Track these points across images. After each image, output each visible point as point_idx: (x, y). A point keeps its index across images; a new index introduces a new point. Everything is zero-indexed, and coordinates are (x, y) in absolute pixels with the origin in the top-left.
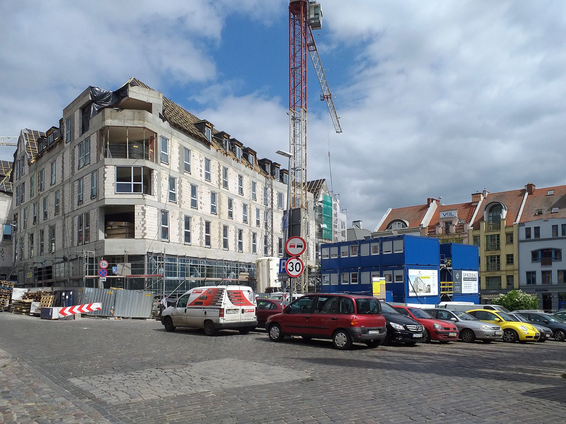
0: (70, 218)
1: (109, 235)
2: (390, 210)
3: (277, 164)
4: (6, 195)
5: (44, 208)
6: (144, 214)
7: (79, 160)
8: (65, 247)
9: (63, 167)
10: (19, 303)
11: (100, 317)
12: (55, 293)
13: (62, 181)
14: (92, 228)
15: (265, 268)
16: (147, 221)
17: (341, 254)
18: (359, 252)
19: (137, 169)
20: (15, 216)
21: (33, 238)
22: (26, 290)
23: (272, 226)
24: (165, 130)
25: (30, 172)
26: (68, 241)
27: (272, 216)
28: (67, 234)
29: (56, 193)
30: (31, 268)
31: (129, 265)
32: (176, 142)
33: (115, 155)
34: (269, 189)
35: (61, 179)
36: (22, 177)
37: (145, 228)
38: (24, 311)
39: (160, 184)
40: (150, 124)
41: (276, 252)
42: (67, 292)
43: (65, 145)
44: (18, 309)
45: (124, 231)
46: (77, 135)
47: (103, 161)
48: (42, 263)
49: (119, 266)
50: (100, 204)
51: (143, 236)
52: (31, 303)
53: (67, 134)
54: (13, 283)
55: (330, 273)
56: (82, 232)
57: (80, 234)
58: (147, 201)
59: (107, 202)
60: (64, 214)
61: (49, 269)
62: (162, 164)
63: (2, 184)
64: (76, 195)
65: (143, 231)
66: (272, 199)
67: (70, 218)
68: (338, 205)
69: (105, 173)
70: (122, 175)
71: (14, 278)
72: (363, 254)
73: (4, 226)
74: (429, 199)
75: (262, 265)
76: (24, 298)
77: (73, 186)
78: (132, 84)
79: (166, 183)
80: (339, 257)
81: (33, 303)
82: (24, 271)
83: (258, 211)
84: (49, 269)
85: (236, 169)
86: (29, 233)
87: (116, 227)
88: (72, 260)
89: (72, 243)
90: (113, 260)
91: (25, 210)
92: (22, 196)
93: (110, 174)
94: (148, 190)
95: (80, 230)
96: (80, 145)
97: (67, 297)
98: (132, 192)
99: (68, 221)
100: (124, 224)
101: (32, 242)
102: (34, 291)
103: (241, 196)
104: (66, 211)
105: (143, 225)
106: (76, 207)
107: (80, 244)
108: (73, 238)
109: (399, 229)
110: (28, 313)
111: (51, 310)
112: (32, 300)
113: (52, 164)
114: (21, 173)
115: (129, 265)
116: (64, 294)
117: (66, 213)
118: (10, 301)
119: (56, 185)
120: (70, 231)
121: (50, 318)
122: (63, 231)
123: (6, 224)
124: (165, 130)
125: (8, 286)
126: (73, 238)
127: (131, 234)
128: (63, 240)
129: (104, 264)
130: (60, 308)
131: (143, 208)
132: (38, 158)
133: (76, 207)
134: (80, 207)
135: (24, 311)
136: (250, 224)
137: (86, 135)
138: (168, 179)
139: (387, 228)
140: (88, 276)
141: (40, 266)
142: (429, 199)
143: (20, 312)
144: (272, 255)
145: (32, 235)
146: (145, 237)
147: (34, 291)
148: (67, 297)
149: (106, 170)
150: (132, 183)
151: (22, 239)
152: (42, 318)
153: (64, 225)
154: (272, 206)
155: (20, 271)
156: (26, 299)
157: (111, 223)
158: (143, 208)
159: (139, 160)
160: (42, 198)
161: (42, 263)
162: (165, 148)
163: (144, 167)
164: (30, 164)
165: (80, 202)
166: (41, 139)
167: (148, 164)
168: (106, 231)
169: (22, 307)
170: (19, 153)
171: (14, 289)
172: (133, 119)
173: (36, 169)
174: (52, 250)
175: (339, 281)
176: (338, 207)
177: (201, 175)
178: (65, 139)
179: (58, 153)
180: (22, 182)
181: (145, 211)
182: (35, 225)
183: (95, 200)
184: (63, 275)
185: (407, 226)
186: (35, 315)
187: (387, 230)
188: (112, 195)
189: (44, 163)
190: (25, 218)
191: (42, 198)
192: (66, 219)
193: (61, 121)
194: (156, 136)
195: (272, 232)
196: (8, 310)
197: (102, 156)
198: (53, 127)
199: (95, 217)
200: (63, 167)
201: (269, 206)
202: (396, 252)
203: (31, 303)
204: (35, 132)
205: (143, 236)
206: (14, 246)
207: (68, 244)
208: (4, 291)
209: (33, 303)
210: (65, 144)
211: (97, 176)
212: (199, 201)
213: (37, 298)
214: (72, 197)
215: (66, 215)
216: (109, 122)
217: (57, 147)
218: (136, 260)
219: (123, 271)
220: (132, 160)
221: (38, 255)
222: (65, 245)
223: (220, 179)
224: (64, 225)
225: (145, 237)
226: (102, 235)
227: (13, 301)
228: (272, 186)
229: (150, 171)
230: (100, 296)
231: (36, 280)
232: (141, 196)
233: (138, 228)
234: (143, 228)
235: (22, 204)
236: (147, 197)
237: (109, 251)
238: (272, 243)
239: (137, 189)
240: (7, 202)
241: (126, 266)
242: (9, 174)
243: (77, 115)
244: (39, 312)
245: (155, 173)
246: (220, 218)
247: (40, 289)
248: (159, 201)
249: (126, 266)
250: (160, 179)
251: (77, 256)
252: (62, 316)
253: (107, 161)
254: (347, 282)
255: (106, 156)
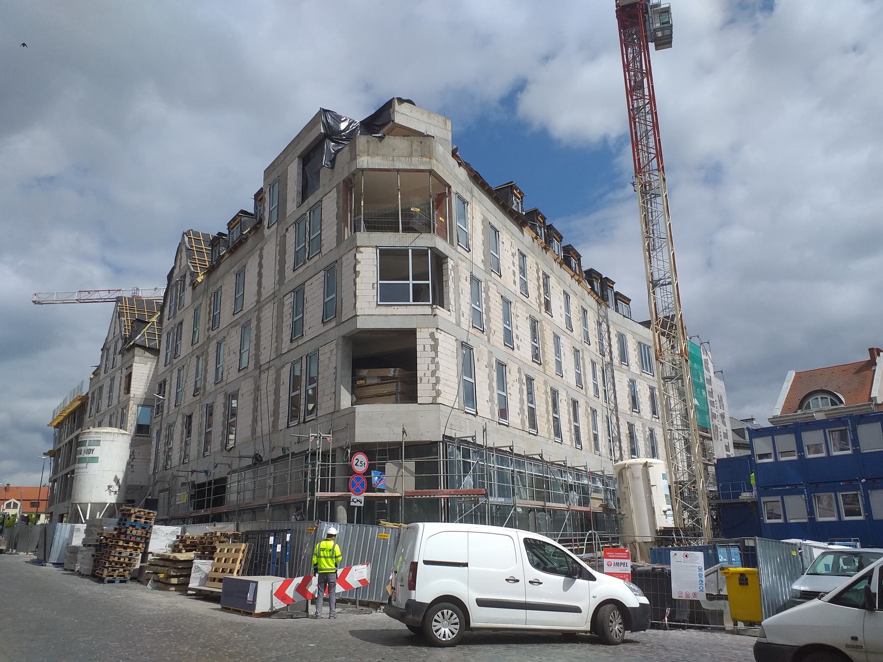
0: (272, 372)
1: (359, 398)
2: (791, 375)
3: (610, 281)
4: (147, 354)
5: (218, 361)
6: (435, 348)
7: (296, 252)
8: (259, 434)
9: (260, 275)
10: (164, 560)
11: (362, 604)
12: (246, 537)
13: (258, 302)
14: (325, 386)
15: (641, 484)
16: (439, 365)
17: (806, 449)
18: (856, 442)
19: (420, 254)
20: (160, 385)
21: (190, 424)
22: (178, 529)
23: (615, 397)
24: (461, 183)
25: (194, 300)
26: (265, 422)
27: (613, 377)
28: (264, 407)
29: (244, 327)
30: (183, 484)
31: (411, 465)
32: (480, 212)
33: (373, 226)
34: (604, 326)
35: (256, 298)
36: (178, 312)
37: (438, 380)
38: (174, 581)
39: (458, 288)
40: (440, 166)
41: (627, 453)
42: (279, 534)
43: (267, 232)
44: (162, 576)
45: (391, 388)
46: (291, 206)
47: (353, 239)
48: (206, 472)
49: (390, 467)
50: (345, 330)
51: (435, 398)
52: (190, 562)
53: (270, 212)
54: (154, 514)
55: (782, 494)
56: (299, 395)
57: (294, 403)
58: (440, 320)
59: (362, 324)
60: (258, 366)
61: (219, 487)
62: (459, 248)
63: (143, 335)
64: (288, 321)
65: (435, 385)
66: (610, 345)
67: (272, 372)
68: (710, 362)
69: (356, 262)
70: (391, 263)
71: (151, 504)
72: (866, 449)
73: (140, 408)
74: (871, 350)
75: (633, 478)
76: (175, 548)
77: (282, 305)
78: (401, 101)
79: (466, 286)
80: (802, 457)
81: (197, 562)
82: (170, 492)
83: (593, 364)
84: (219, 487)
85: (560, 279)
86: (183, 415)
87: (375, 381)
88: (274, 461)
89: (275, 424)
90: (381, 453)
91: (179, 371)
92: (177, 346)
93: (368, 263)
94: (440, 300)
95: (293, 394)
96: (297, 223)
97: (279, 548)
98: (411, 302)
99: (267, 380)
100: (391, 372)
101: (189, 433)
102: (196, 531)
103: (569, 332)
104: (264, 358)
105: (433, 373)
106: (286, 346)
107: (295, 422)
108: (276, 414)
109: (826, 408)
110: (183, 588)
111: (252, 586)
112: (191, 555)
113: (238, 275)
114: (179, 304)
115: (411, 465)
116: (272, 539)
117: (262, 363)
118: (145, 554)
119: (244, 311)
120: (271, 398)
121: (248, 610)
122: (256, 399)
123: (143, 406)
124: (461, 183)
125: (143, 520)
126: (276, 414)
127: (410, 395)
128: (255, 420)
129: (360, 463)
130: (278, 581)
131: (432, 335)
132: (210, 271)
133: (286, 346)
134: (295, 344)
135: (174, 581)
136: (586, 391)
137: (311, 200)
138: (469, 279)
139: (800, 407)
140: (318, 494)
141: (202, 478)
142: (871, 350)
143: (163, 585)
144: (654, 454)
145: (190, 417)
146: (439, 400)
147: (196, 531)
148: (279, 548)
149: (358, 256)
150: (411, 282)
151: (170, 426)
152: (225, 609)
153: (257, 389)
154: (611, 359)
155: (160, 491)
156: (180, 551)
157: (364, 372)
158: (432, 335)
159: (423, 235)
160: (215, 341)
161: (206, 472)
162: (463, 217)
163: (431, 248)
164: (194, 285)
165: (297, 329)
166: (216, 241)
167: (441, 245)
168: (354, 390)
169: (171, 573)
170: (176, 271)
171: (155, 527)
172: (411, 155)
173: (206, 290)
174: (227, 443)
175: (811, 512)
176: (710, 366)
177: (515, 282)
178: (266, 223)
179: (251, 252)
180: (178, 320)
181: (436, 340)
182: (198, 397)
183: (333, 324)
184: (248, 495)
185: (841, 402)
186: (202, 596)
187: (799, 412)
188: (370, 310)
189: (223, 277)
190: (178, 387)
191: (215, 341)
192: (264, 376)
193: (259, 197)
194: (450, 192)
195: (617, 411)
196: (138, 577)
197: (347, 233)
198: (242, 212)
199: (332, 360)
200: (260, 275)
201: (607, 359)
202: (782, 459)
203: (190, 562)
204: (206, 236)
205: (435, 398)
206: (154, 442)
207: (265, 426)
208: (134, 532)
209: (197, 562)
210: (266, 229)
211: (335, 279)
212: (515, 332)
213: (206, 549)
214: (279, 328)
215: (263, 368)
216: (364, 161)
217: (250, 240)
218: (422, 452)
219: (398, 480)
220: (411, 236)
221: (199, 457)
222: (259, 430)
223: (540, 295)
224: (257, 389)
225: (439, 400)
226: (346, 399)
227: (150, 557)
228: (607, 320)
229: (440, 259)
230: (358, 546)
231: (191, 509)
232: (428, 310)
233: (425, 380)
234: (433, 380)
235: (175, 361)
236: (440, 311)
237: (364, 433)
238: (619, 432)
239: (420, 294)
240: (148, 366)
241: (406, 469)
242: (154, 319)
243: (294, 170)
244: (217, 588)
245: (450, 263)
246: (545, 372)
247: (208, 528)
248: (458, 324)
249: (406, 469)
250: (457, 279)
251: (284, 449)
252: (279, 604)
253: (362, 237)
254: (778, 517)
255: (356, 229)
